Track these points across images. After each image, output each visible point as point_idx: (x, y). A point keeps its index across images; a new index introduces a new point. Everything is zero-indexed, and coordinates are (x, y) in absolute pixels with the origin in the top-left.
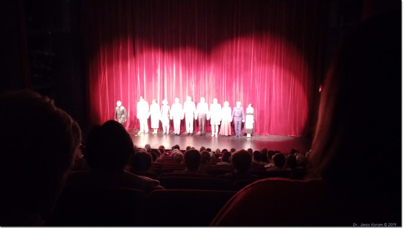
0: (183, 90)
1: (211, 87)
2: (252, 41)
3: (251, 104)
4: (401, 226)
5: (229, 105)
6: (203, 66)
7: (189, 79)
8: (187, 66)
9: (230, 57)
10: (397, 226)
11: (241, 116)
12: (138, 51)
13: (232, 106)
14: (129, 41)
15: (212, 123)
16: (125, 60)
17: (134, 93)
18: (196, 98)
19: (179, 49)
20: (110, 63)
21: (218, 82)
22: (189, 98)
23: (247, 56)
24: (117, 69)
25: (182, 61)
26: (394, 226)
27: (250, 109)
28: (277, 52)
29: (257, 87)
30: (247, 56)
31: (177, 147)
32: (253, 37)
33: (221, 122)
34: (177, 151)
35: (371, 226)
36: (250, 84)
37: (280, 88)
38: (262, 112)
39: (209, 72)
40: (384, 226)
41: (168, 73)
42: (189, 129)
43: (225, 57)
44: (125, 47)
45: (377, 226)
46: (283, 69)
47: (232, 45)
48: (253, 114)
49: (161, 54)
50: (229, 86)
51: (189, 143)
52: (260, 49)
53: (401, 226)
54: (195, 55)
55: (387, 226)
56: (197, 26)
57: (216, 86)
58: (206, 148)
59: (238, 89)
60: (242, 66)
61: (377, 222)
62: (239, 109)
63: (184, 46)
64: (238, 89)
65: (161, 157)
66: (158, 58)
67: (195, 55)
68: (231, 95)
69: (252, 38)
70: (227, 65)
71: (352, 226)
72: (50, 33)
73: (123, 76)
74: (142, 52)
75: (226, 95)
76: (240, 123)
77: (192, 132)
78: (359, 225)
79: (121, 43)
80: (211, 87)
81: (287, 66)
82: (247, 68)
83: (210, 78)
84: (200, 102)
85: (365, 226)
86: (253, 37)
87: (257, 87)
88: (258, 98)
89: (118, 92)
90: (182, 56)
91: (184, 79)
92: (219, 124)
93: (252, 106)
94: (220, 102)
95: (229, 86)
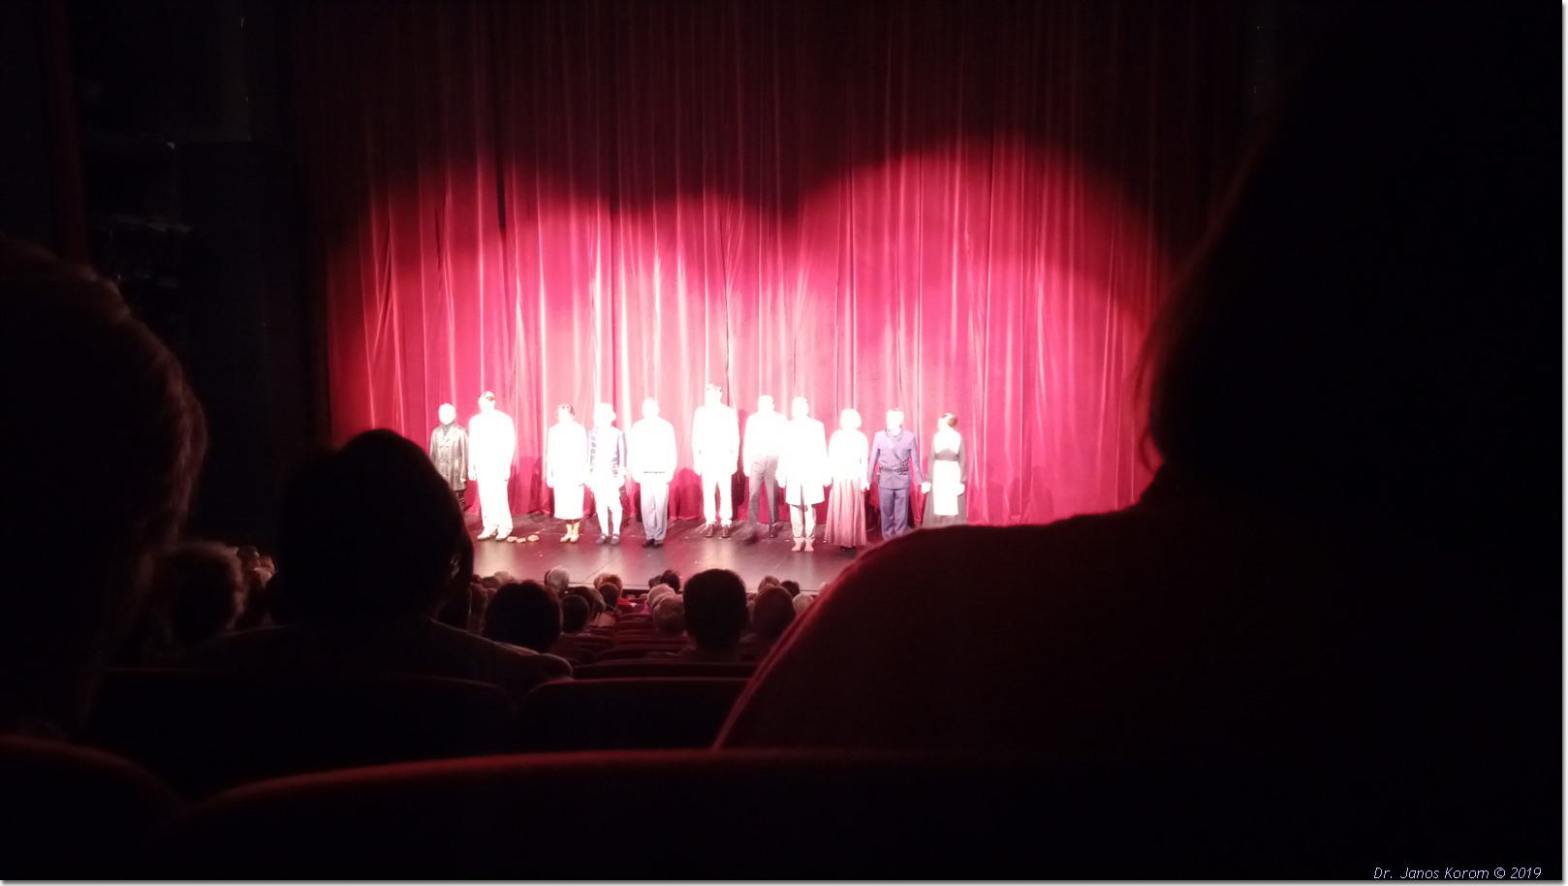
0: (693, 362)
1: (801, 347)
2: (953, 170)
3: (950, 416)
4: (1559, 878)
5: (859, 423)
6: (770, 266)
7: (713, 311)
8: (706, 270)
9: (869, 232)
10: (1545, 877)
11: (905, 468)
12: (515, 213)
13: (873, 424)
14: (480, 180)
15: (791, 498)
16: (466, 246)
17: (503, 376)
18: (743, 392)
19: (674, 199)
20: (409, 263)
21: (827, 332)
22: (713, 394)
23: (934, 227)
24: (437, 284)
25: (688, 248)
26: (1533, 878)
27: (947, 438)
28: (1051, 208)
29: (977, 344)
30: (934, 227)
31: (670, 579)
32: (959, 154)
33: (827, 491)
34: (668, 593)
35: (1441, 878)
36: (948, 337)
37: (1065, 340)
38: (995, 436)
39: (791, 287)
40: (1492, 878)
41: (633, 295)
42: (717, 510)
43: (851, 226)
44: (466, 200)
45: (1466, 878)
46: (1076, 277)
47: (879, 187)
48: (957, 457)
49: (603, 231)
50: (869, 338)
51: (717, 557)
52: (985, 190)
53: (1559, 878)
54: (735, 228)
55: (1507, 878)
56: (744, 129)
57: (818, 344)
58: (782, 580)
59: (903, 351)
60: (919, 267)
61: (1466, 864)
62: (898, 438)
63: (694, 191)
64: (903, 351)
65: (604, 620)
66: (591, 236)
67: (735, 228)
68: (877, 378)
69: (953, 158)
70: (861, 264)
71: (1368, 877)
72: (172, 145)
73: (458, 329)
74: (529, 215)
75: (860, 379)
76: (902, 494)
77: (726, 521)
78: (1396, 876)
79: (450, 185)
80: (801, 347)
81: (1090, 266)
82: (935, 275)
83: (795, 313)
84: (755, 409)
85: (1420, 879)
86: (959, 154)
87: (977, 344)
88: (980, 392)
89: (440, 372)
90: (687, 233)
91: (696, 321)
92: (820, 499)
93: (954, 423)
94: (829, 419)
95: (869, 338)
